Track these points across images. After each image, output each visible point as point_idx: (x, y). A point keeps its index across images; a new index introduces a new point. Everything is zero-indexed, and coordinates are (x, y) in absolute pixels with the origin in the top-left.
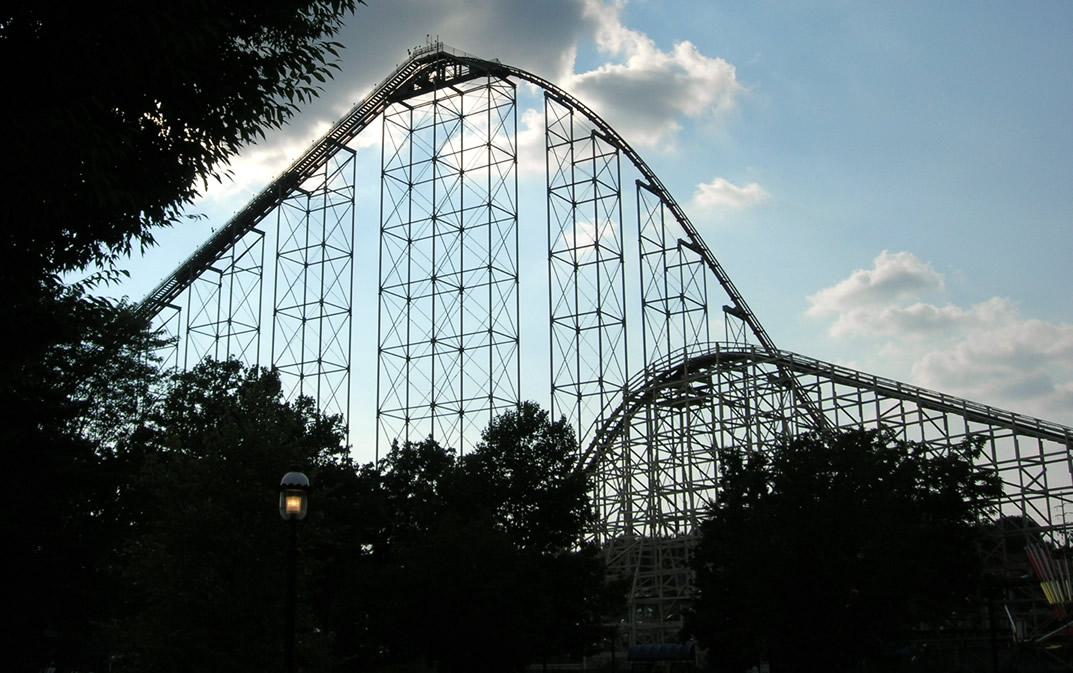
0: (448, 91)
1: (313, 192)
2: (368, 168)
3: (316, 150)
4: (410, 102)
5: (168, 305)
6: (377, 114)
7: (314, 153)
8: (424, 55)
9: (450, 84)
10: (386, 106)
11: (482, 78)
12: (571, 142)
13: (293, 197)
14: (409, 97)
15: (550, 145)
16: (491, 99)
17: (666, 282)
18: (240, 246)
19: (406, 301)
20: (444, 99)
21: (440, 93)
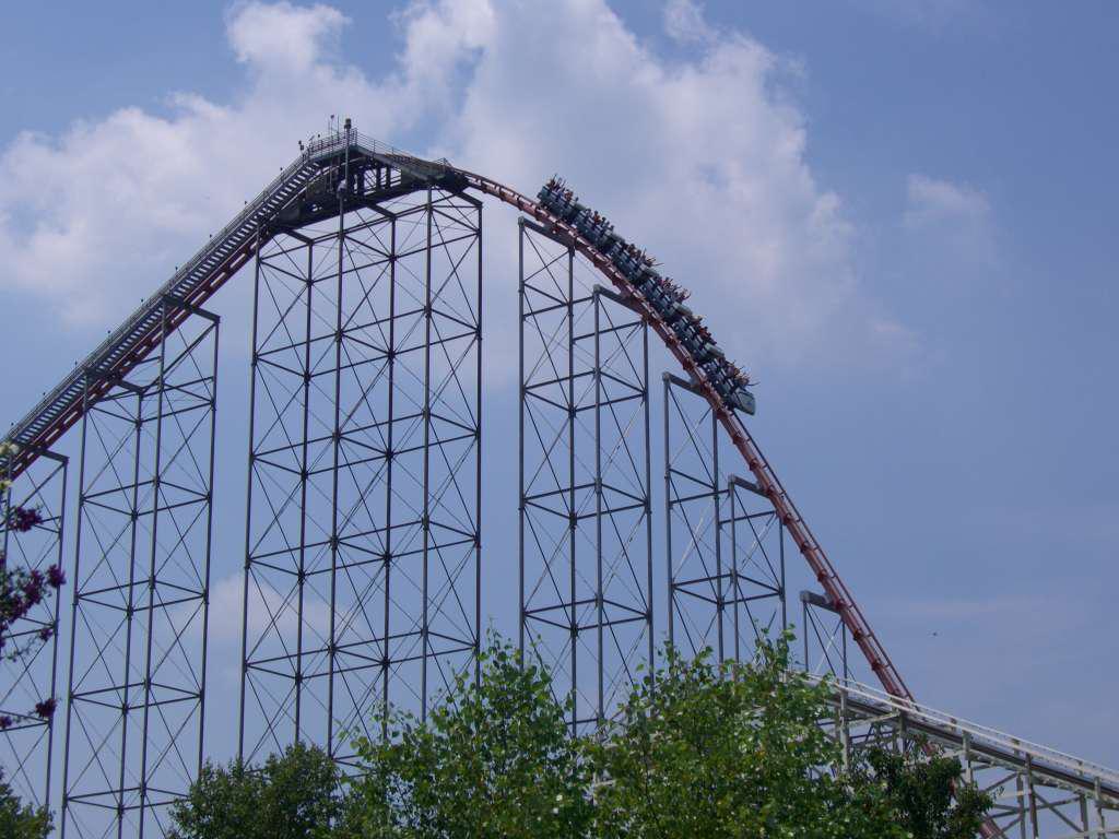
0: (367, 213)
1: (148, 388)
2: (235, 342)
3: (148, 317)
4: (309, 231)
5: (197, 310)
6: (250, 254)
7: (144, 320)
8: (325, 152)
9: (371, 202)
10: (266, 239)
11: (416, 193)
12: (570, 304)
13: (111, 398)
14: (301, 224)
15: (526, 311)
16: (434, 229)
17: (387, 597)
18: (174, 344)
19: (297, 578)
20: (358, 228)
21: (351, 219)
